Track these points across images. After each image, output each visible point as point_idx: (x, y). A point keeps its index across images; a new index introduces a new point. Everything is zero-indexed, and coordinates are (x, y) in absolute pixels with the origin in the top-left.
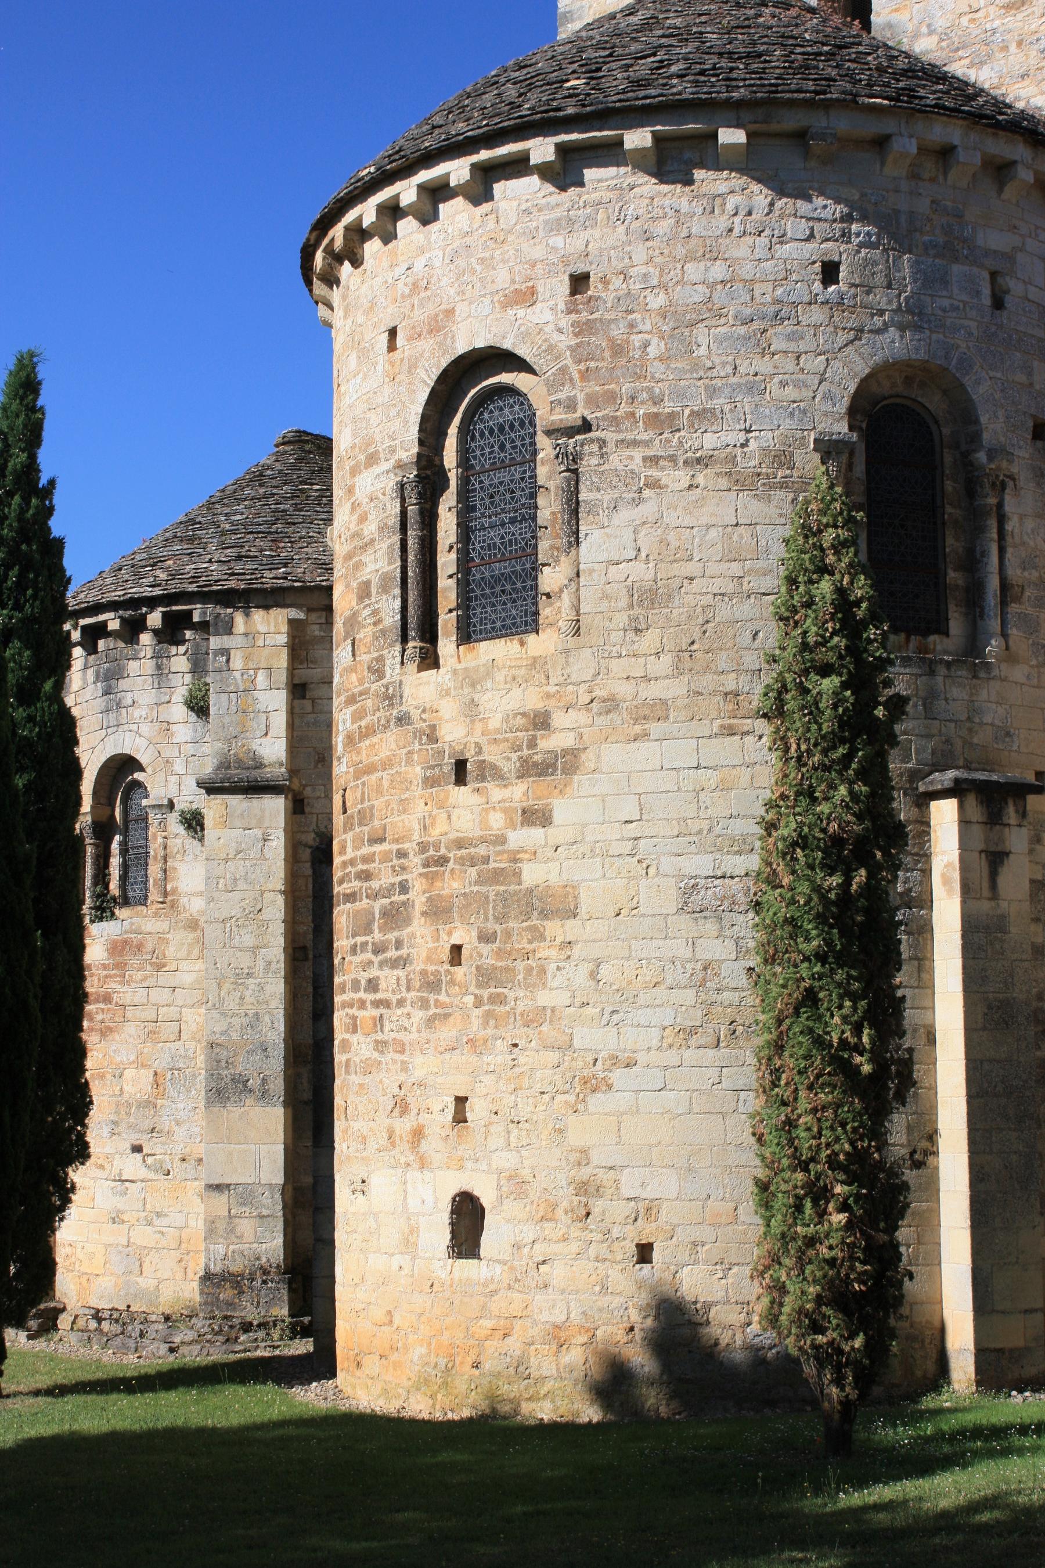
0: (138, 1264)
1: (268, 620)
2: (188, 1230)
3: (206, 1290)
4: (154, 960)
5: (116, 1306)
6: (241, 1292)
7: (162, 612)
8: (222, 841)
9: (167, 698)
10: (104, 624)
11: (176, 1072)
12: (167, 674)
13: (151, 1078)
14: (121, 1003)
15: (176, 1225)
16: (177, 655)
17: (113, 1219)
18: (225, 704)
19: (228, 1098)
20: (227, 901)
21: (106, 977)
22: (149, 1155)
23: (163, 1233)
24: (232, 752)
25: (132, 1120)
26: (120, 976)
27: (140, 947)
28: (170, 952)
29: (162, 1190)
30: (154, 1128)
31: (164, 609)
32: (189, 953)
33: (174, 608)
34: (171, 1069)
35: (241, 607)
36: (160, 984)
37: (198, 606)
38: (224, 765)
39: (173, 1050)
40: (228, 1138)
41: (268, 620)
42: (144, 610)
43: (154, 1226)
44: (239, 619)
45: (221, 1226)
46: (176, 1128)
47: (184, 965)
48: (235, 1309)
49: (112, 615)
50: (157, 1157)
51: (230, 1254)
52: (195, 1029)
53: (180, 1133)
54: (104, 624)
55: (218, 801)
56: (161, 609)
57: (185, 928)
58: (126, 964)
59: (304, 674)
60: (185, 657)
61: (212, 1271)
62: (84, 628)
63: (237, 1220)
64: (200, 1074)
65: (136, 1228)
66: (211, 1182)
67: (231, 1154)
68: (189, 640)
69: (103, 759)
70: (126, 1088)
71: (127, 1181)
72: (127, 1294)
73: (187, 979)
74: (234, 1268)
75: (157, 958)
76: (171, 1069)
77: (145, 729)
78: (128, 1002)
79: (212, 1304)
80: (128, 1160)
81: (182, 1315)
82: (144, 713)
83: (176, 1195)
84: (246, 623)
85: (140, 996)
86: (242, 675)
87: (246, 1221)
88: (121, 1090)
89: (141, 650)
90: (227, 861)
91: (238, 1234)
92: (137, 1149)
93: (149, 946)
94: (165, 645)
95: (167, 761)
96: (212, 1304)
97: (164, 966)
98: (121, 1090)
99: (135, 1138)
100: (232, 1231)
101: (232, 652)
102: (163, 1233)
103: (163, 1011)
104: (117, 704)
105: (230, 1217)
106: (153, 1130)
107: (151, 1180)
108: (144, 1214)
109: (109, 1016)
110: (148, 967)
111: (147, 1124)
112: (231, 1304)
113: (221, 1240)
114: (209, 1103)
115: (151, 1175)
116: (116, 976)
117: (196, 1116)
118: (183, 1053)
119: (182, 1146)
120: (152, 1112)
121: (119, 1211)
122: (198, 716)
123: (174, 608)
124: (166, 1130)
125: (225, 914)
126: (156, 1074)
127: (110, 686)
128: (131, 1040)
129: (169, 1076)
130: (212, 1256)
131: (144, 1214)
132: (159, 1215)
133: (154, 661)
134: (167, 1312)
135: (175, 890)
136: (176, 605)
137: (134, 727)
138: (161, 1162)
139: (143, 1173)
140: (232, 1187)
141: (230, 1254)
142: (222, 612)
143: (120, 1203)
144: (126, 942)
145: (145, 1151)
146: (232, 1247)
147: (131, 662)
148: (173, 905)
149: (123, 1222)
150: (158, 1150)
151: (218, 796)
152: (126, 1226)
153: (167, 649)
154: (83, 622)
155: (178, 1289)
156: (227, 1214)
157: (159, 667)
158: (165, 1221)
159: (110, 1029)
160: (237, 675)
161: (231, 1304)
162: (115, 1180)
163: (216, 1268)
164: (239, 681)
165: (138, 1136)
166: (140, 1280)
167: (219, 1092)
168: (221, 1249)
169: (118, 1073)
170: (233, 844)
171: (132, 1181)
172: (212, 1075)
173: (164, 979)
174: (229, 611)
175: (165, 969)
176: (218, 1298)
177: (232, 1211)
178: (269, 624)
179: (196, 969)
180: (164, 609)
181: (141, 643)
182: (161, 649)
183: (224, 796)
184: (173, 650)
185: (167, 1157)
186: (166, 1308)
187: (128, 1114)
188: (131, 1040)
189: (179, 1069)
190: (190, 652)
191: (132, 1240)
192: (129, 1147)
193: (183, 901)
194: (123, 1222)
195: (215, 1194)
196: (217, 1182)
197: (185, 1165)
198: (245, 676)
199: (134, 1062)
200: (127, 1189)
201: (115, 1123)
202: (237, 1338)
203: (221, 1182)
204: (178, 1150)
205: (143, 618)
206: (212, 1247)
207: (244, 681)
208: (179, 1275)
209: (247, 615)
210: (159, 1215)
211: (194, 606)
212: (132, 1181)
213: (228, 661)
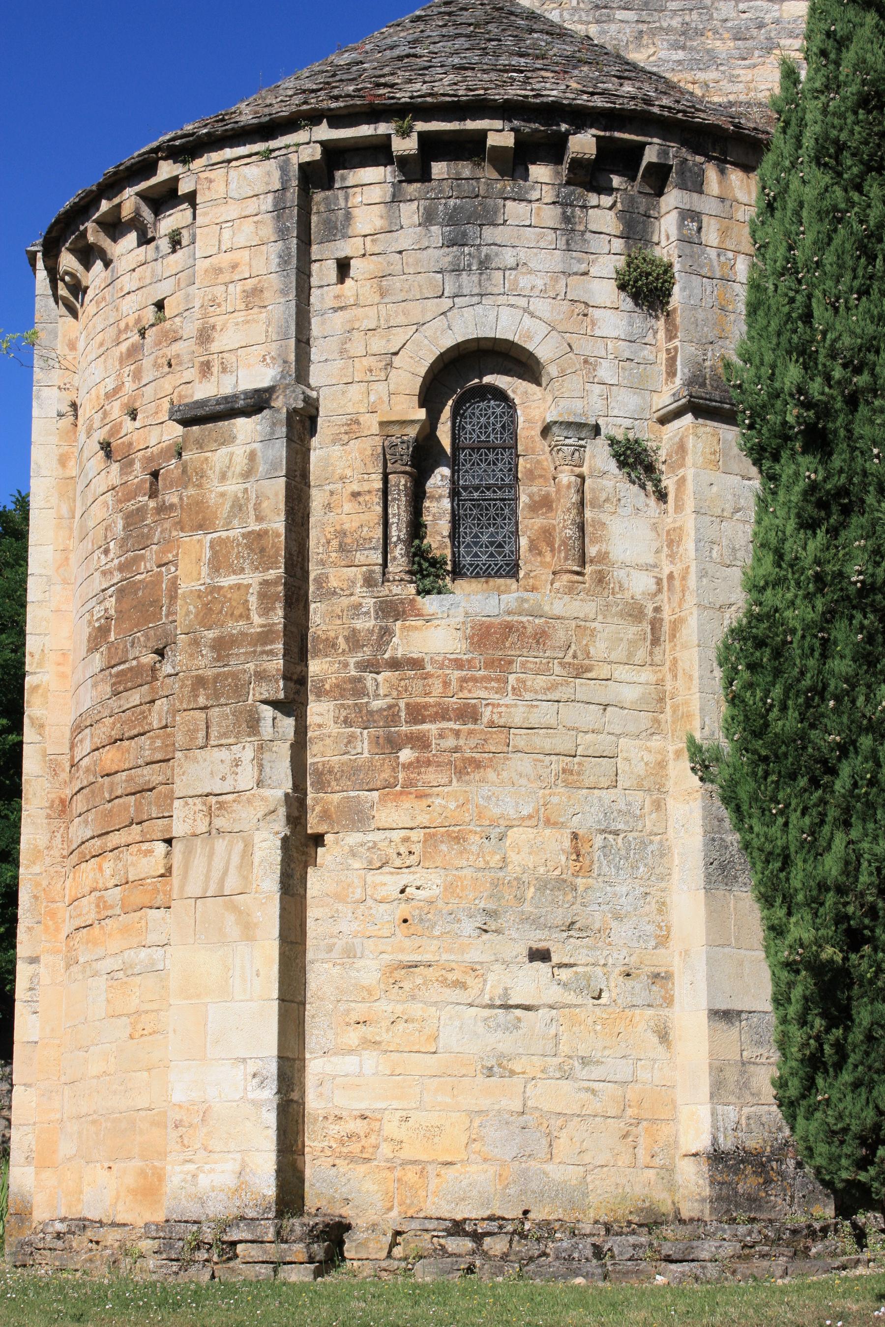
0: (544, 1142)
1: (748, 186)
2: (638, 1086)
3: (719, 1178)
4: (568, 659)
5: (499, 1213)
6: (768, 1181)
7: (598, 138)
8: (715, 489)
9: (583, 267)
10: (482, 135)
11: (610, 837)
12: (583, 233)
13: (567, 844)
14: (502, 722)
15: (618, 1078)
16: (598, 206)
17: (491, 1069)
18: (697, 291)
19: (735, 877)
20: (724, 579)
21: (464, 680)
22: (560, 966)
23: (594, 1092)
24: (708, 363)
25: (527, 908)
26: (498, 680)
27: (541, 637)
28: (599, 649)
29: (590, 1021)
30: (573, 923)
31: (602, 133)
32: (630, 655)
33: (617, 134)
34: (604, 831)
35: (715, 158)
36: (579, 697)
37: (656, 140)
38: (695, 380)
39: (607, 802)
40: (737, 939)
41: (748, 186)
42: (564, 127)
43: (576, 1080)
44: (711, 173)
45: (732, 1076)
46: (614, 924)
47: (621, 672)
48: (760, 1208)
49: (498, 124)
50: (579, 969)
51: (743, 1121)
52: (642, 773)
53: (621, 932)
54: (482, 135)
55: (708, 429)
56: (594, 131)
57: (621, 614)
58: (511, 663)
59: (300, 337)
60: (612, 213)
61: (722, 1148)
62: (422, 135)
63: (752, 1068)
64: (651, 842)
65: (540, 1083)
66: (717, 1007)
67: (741, 964)
68: (618, 190)
69: (448, 342)
70: (513, 856)
71: (517, 1007)
72: (523, 1192)
73: (629, 694)
74: (752, 1144)
75: (574, 657)
76: (604, 831)
77: (540, 306)
78: (518, 721)
79: (728, 1200)
80: (521, 973)
81: (630, 1223)
82: (540, 283)
83: (617, 1030)
84: (720, 183)
85: (544, 713)
86: (719, 255)
87: (764, 1068)
88: (504, 859)
89: (533, 188)
90: (722, 519)
91: (754, 1091)
92: (540, 955)
93: (560, 636)
94: (579, 190)
95: (586, 362)
96: (728, 1200)
97: (589, 669)
98: (504, 859)
99: (538, 939)
100: (746, 1085)
101: (705, 219)
102: (594, 1092)
103: (582, 739)
104: (481, 263)
105: (743, 1064)
106: (570, 926)
107: (569, 1006)
108: (556, 1061)
109: (472, 742)
110: (558, 670)
111: (560, 916)
112: (755, 1200)
113: (732, 1099)
114: (710, 883)
115: (570, 998)
116: (490, 679)
117: (647, 907)
118: (624, 808)
119: (624, 952)
120: (570, 897)
121: (502, 1055)
122: (637, 304)
123: (617, 134)
124: (597, 926)
125: (721, 600)
126: (575, 836)
127: (464, 234)
128: (523, 781)
129: (598, 840)
130: (720, 1124)
131: (556, 1061)
132: (585, 1061)
133: (558, 210)
134: (604, 1218)
135: (603, 557)
136: (620, 131)
137: (522, 302)
138: (588, 978)
139: (554, 994)
140: (744, 1016)
141: (743, 1121)
142: (689, 158)
143: (505, 1043)
144: (509, 628)
145: (555, 959)
146: (746, 1110)
147: (509, 203)
148: (601, 579)
149: (512, 1073)
150: (581, 957)
151: (708, 422)
152: (518, 1080)
153: (581, 196)
154: (421, 126)
155: (624, 1181)
156: (738, 1058)
157: (567, 219)
158: (597, 1072)
159: (478, 765)
160: (713, 253)
161: (755, 1200)
162: (492, 1006)
163: (727, 1144)
164: (715, 263)
165: (539, 935)
166: (549, 1167)
167: (723, 868)
168: (731, 1113)
169: (494, 833)
170: (730, 497)
171: (527, 1008)
172: (713, 840)
173: (583, 688)
174: (699, 159)
175: (589, 675)
176: (735, 1190)
177: (745, 1053)
178: (749, 193)
179: (642, 679)
180: (602, 133)
181: (531, 178)
182: (572, 193)
183: (716, 424)
184: (593, 199)
185: (599, 971)
186: (602, 1212)
187: (521, 900)
188: (523, 781)
189: (616, 833)
190: (619, 205)
191: (530, 1103)
192: (525, 952)
193: (619, 574)
194: (512, 1073)
195: (722, 1025)
196: (724, 1007)
197: (630, 983)
198: (722, 259)
199: (530, 817)
200: (519, 1019)
201: (492, 914)
202: (808, 1249)
203: (729, 1007)
204: (618, 958)
205: (562, 141)
206: (719, 1107)
207: (722, 265)
208: (624, 1160)
209: (722, 172)
210: (585, 1061)
211: (650, 140)
212: (527, 1008)
213: (700, 229)
